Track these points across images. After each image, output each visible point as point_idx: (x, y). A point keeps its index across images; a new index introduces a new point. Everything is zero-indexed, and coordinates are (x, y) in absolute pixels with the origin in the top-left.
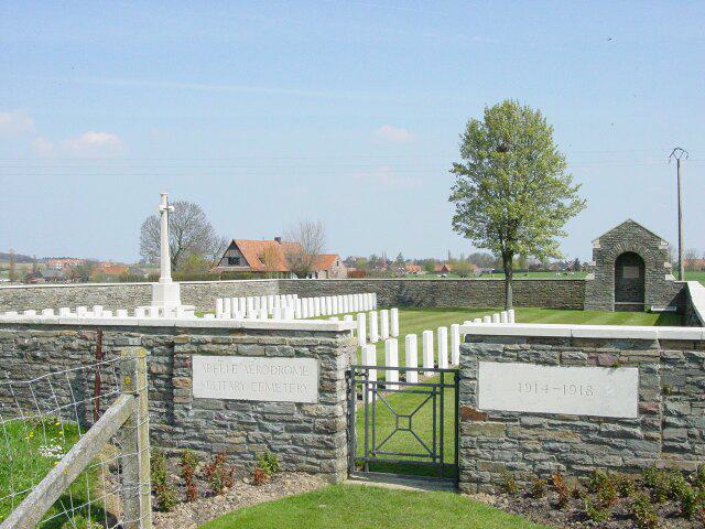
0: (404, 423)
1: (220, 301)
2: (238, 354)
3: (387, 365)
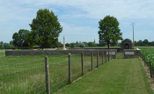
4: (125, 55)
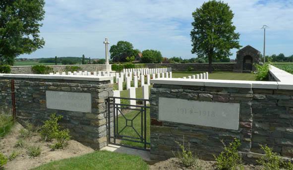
0: (129, 123)
1: (124, 69)
2: (61, 90)
3: (131, 97)
4: (155, 122)
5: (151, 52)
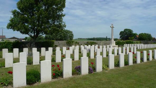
1: (125, 45)
5: (145, 34)
